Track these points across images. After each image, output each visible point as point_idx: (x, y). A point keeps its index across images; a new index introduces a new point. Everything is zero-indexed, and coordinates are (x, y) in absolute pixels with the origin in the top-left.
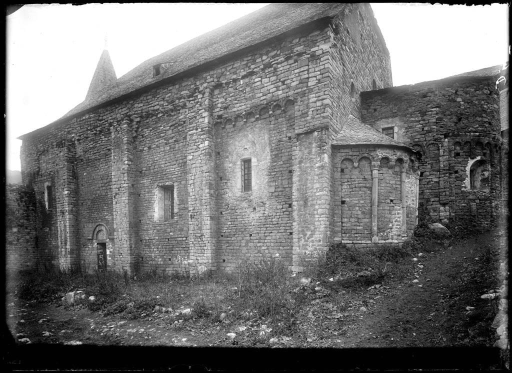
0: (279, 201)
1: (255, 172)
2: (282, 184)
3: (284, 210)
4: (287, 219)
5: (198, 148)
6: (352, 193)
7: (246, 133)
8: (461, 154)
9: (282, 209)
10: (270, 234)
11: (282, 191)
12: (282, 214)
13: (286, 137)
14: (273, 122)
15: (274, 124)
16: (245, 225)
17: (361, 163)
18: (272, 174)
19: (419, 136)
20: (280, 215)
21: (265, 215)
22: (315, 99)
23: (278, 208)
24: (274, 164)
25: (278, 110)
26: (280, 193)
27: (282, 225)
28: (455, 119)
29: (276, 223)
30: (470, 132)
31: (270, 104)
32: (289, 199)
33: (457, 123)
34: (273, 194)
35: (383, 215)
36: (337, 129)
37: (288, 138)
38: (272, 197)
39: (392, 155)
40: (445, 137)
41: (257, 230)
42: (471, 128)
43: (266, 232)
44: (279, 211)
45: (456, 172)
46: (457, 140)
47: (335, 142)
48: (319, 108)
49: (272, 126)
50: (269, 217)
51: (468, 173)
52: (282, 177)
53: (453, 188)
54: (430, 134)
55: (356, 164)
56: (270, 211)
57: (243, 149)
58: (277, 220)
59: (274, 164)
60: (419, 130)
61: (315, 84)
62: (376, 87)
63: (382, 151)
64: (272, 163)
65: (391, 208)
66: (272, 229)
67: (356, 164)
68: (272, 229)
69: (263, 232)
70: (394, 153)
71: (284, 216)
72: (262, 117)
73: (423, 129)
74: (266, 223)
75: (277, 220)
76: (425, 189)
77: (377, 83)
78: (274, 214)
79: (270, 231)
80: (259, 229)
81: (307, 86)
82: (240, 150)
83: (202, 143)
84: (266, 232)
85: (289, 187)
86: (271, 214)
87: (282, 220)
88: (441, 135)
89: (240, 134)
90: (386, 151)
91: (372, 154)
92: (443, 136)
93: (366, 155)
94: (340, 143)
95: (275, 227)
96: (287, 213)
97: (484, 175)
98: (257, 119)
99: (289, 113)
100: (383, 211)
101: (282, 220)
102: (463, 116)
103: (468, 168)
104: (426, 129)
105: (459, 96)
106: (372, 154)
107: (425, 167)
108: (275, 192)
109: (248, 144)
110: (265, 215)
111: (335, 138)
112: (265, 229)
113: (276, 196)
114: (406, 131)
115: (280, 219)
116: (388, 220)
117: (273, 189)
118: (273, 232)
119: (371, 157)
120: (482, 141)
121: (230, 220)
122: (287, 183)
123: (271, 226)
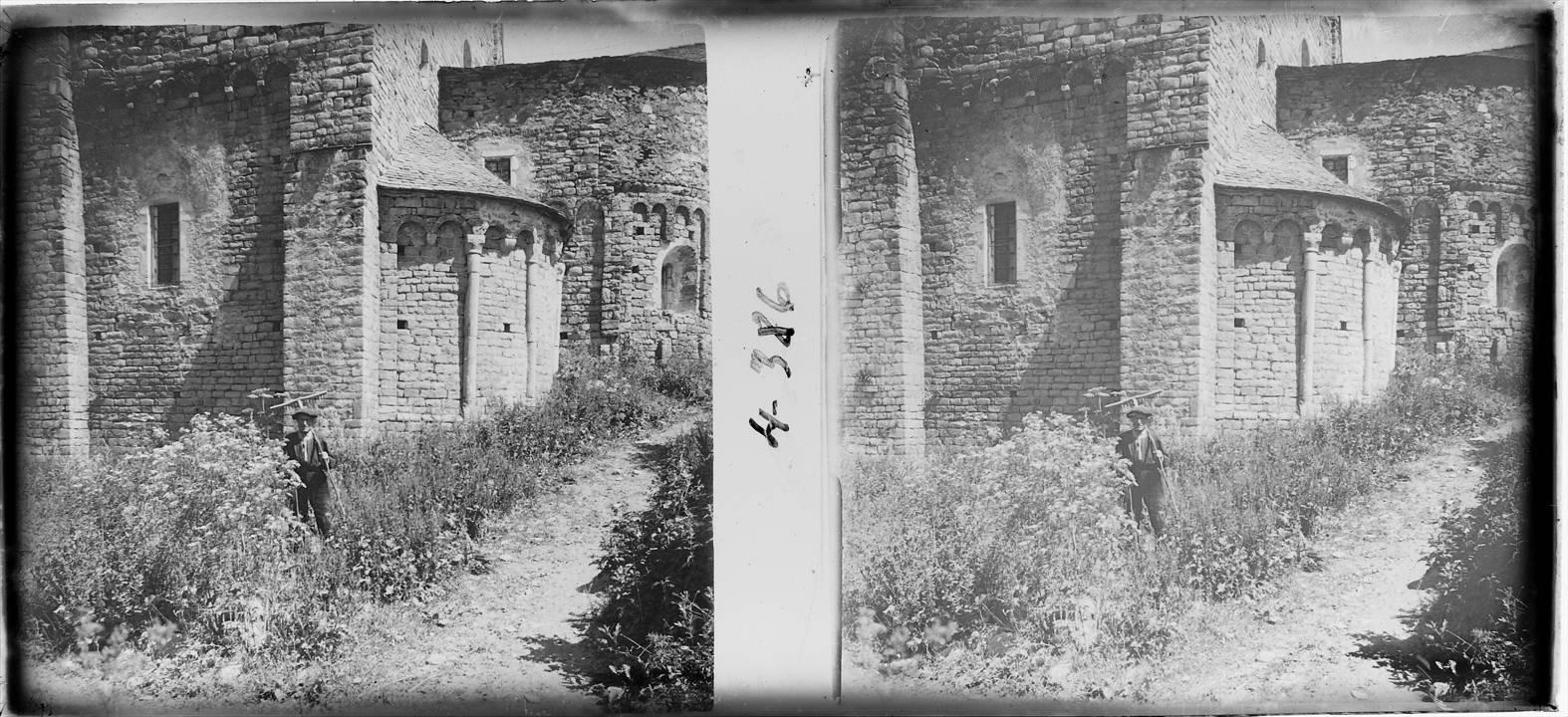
0: (1089, 312)
1: (1025, 235)
2: (1093, 272)
3: (1097, 334)
4: (269, 358)
5: (868, 159)
6: (1258, 301)
7: (164, 135)
8: (1481, 230)
9: (1094, 331)
10: (228, 394)
11: (1093, 288)
12: (257, 345)
13: (1105, 155)
14: (234, 116)
15: (1073, 119)
16: (164, 368)
17: (1279, 234)
18: (1070, 243)
19: (562, 184)
20: (251, 349)
21: (215, 346)
22: (1179, 67)
23: (1084, 329)
24: (1074, 220)
25: (1084, 83)
26: (253, 294)
27: (257, 372)
28: (1472, 151)
29: (1078, 365)
30: (664, 183)
31: (1062, 65)
32: (1112, 307)
33: (640, 161)
34: (1072, 295)
35: (489, 358)
36: (391, 152)
37: (1108, 158)
38: (232, 303)
39: (510, 223)
40: (616, 192)
41: (1029, 382)
42: (1503, 174)
43: (1054, 386)
44: (248, 338)
45: (635, 270)
46: (1476, 198)
47: (1222, 181)
48: (1187, 91)
49: (232, 124)
50: (1060, 351)
51: (1494, 272)
52: (1095, 253)
53: (629, 304)
54: (1423, 180)
55: (1268, 237)
56: (228, 338)
57: (991, 174)
58: (1081, 358)
59: (1074, 220)
60: (564, 169)
61: (1174, 29)
62: (470, 61)
63: (490, 212)
64: (232, 217)
65: (1343, 341)
66: (1068, 379)
67: (431, 238)
68: (1068, 379)
69: (210, 387)
70: (515, 218)
71: (262, 351)
72: (1043, 98)
73: (572, 168)
74: (215, 367)
75: (1081, 358)
76: (571, 302)
77: (1310, 49)
78: (1074, 344)
79: (1062, 386)
80: (1036, 379)
81: (1158, 33)
82: (985, 176)
83: (876, 148)
84: (217, 387)
85: (274, 280)
86: (1066, 344)
87: (1093, 360)
88: (608, 185)
89: (985, 136)
90: (498, 213)
91: (468, 216)
92: (612, 188)
93: (1290, 215)
94: (1234, 183)
95: (239, 376)
96: (271, 344)
97: (687, 278)
98: (1029, 103)
99: (277, 96)
100: (489, 350)
101: (1093, 360)
102: (653, 147)
103: (1494, 262)
104: (579, 167)
105: (1483, 101)
106: (468, 216)
107: (573, 254)
108: (1076, 288)
109: (170, 163)
110: (215, 346)
111: (384, 171)
112: (213, 381)
113: (240, 301)
114: (1373, 167)
115: (252, 358)
116: (498, 370)
117: (1067, 281)
118: (233, 387)
119: (1301, 223)
120: (687, 205)
121: (958, 353)
122: (269, 270)
123: (228, 373)
